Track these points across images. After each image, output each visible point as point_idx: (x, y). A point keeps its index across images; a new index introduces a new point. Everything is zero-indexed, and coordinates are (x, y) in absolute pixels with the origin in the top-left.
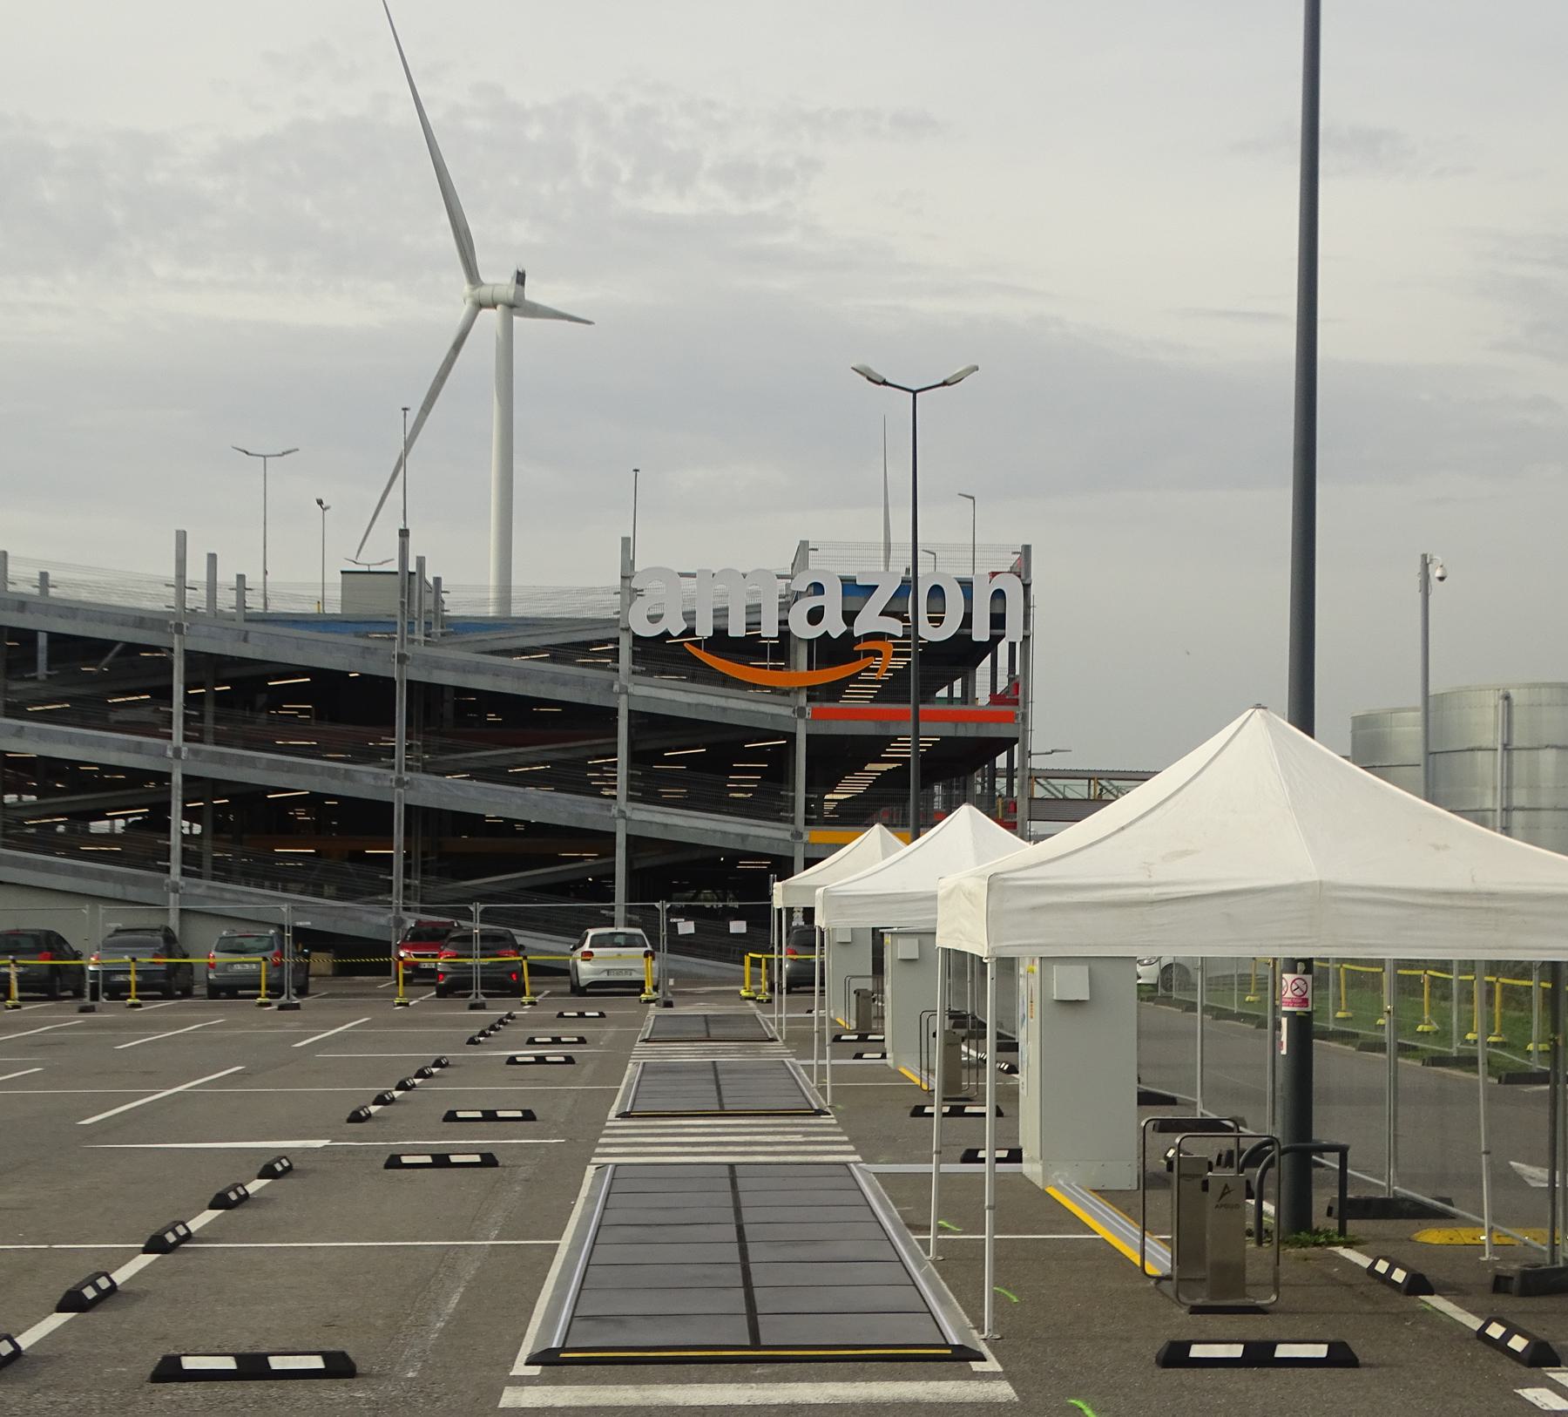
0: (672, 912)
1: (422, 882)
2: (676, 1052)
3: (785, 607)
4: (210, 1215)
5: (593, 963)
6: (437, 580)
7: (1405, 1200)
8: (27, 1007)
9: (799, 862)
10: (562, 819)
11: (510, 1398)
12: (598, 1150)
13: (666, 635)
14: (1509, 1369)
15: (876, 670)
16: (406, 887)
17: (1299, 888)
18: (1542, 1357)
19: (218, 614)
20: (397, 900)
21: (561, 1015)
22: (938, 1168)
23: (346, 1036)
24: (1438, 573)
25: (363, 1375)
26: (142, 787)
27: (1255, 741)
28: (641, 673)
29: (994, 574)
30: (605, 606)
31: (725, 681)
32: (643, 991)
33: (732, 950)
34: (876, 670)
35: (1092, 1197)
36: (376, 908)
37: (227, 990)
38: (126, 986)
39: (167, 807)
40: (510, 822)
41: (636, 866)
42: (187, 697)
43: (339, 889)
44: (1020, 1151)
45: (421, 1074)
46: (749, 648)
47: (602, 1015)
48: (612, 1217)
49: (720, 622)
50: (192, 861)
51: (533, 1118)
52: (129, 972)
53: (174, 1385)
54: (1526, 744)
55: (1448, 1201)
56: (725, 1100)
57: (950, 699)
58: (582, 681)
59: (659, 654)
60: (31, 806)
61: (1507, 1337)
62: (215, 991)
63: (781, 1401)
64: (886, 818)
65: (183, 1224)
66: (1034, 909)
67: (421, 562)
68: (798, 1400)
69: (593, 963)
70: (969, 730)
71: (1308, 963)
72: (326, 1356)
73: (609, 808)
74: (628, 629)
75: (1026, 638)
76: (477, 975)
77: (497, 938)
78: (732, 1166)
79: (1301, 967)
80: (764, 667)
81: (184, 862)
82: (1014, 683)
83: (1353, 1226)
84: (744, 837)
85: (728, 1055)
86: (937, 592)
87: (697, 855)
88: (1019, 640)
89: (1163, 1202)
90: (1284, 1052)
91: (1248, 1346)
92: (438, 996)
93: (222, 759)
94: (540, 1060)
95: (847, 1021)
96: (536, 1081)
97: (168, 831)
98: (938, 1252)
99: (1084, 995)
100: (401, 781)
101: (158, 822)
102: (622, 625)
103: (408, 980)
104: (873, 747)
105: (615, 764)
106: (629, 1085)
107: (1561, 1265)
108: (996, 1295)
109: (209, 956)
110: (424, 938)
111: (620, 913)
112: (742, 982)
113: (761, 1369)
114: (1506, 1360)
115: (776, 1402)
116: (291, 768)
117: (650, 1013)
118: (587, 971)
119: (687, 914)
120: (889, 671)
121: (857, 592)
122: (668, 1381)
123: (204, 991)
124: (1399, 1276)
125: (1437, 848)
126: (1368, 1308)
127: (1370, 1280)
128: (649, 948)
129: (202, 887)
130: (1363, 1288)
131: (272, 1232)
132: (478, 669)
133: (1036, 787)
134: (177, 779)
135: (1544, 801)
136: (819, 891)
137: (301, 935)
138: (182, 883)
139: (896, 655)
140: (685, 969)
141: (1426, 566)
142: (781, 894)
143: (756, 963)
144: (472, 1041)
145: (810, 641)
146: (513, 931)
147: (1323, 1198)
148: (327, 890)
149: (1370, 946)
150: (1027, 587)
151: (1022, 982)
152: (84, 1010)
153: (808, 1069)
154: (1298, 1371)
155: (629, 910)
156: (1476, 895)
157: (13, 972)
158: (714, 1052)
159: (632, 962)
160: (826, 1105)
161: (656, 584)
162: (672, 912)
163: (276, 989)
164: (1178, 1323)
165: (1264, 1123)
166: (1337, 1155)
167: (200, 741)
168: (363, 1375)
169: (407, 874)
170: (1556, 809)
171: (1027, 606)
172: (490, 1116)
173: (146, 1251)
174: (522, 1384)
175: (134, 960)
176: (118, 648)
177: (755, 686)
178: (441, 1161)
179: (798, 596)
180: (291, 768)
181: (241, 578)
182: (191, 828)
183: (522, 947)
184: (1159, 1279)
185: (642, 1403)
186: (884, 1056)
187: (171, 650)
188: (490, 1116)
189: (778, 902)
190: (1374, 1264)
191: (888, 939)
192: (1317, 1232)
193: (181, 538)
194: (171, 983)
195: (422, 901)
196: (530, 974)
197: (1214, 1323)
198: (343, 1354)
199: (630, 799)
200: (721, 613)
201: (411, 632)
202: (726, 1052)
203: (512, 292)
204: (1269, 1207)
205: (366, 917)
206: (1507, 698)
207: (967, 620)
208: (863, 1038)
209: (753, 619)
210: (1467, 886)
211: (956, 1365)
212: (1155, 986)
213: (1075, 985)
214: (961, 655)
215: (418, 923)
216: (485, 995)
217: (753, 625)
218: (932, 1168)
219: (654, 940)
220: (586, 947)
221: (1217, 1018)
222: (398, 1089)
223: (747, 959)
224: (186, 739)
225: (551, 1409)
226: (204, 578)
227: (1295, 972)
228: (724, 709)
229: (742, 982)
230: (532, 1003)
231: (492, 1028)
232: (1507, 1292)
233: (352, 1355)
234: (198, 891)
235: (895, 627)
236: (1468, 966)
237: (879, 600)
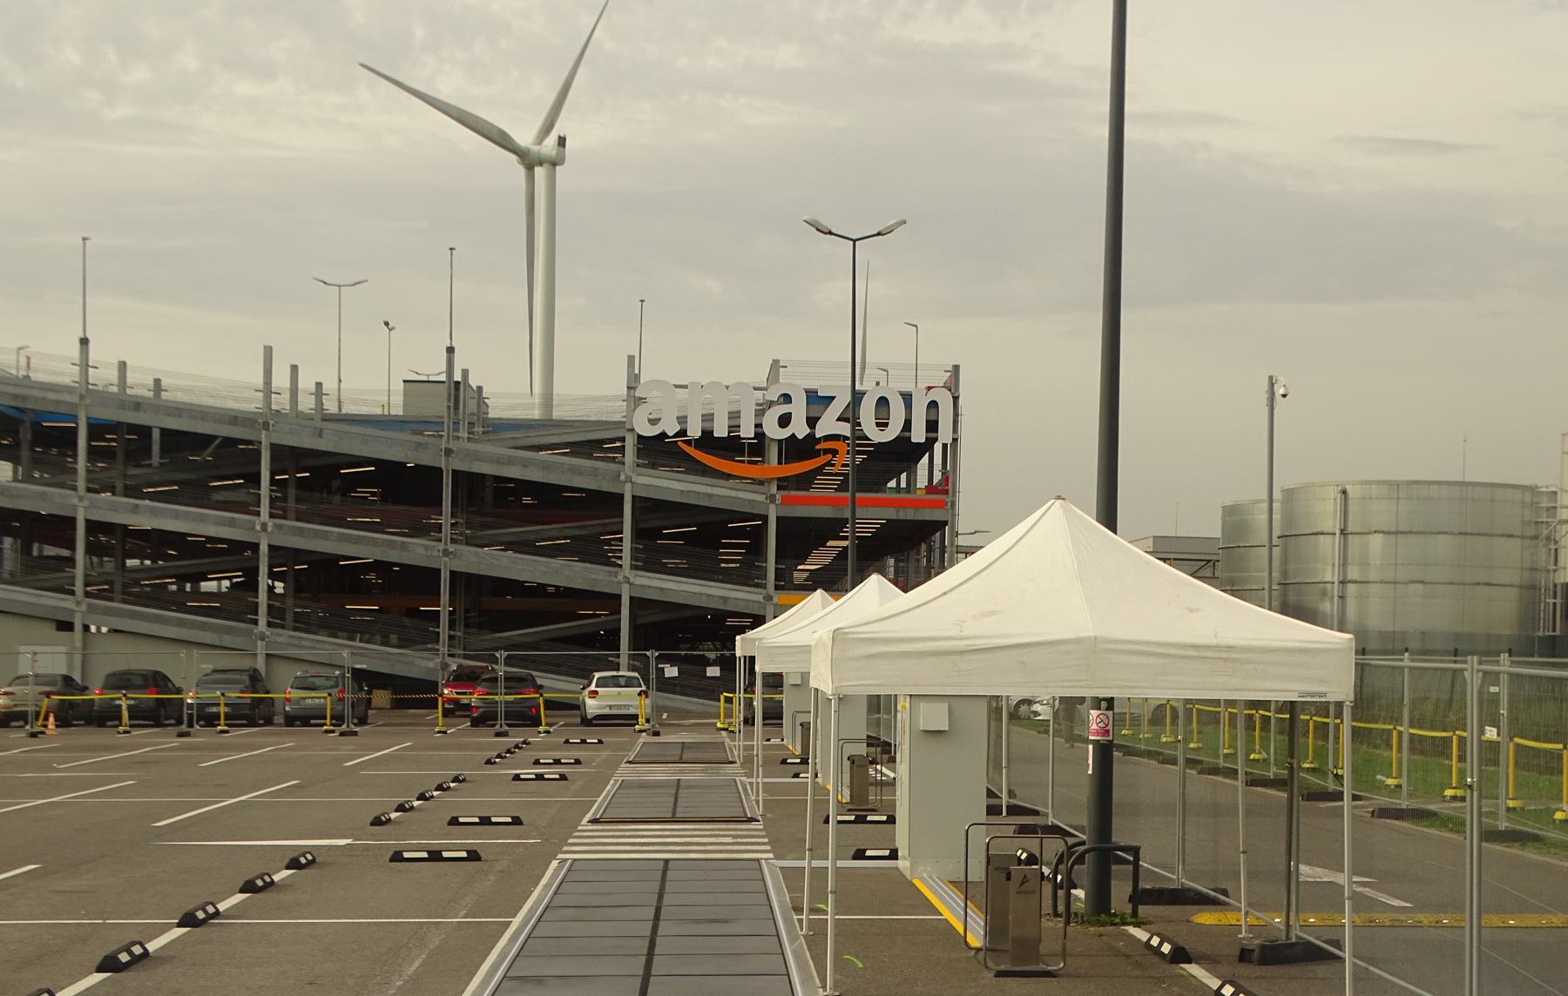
0: (660, 659)
3: (760, 413)
6: (480, 388)
7: (1190, 890)
8: (135, 732)
10: (578, 584)
13: (663, 435)
16: (451, 638)
17: (1078, 641)
19: (300, 415)
20: (443, 648)
21: (567, 742)
22: (834, 864)
23: (390, 755)
24: (1282, 391)
26: (238, 554)
28: (644, 466)
29: (929, 388)
30: (615, 411)
31: (705, 471)
33: (710, 691)
37: (302, 719)
38: (217, 716)
40: (542, 587)
42: (273, 482)
45: (440, 788)
46: (731, 446)
47: (600, 742)
48: (558, 901)
49: (708, 425)
50: (277, 616)
51: (520, 823)
55: (1225, 892)
57: (898, 489)
58: (594, 472)
59: (658, 450)
60: (148, 569)
62: (290, 721)
67: (465, 373)
70: (909, 514)
71: (1110, 702)
75: (955, 440)
76: (501, 709)
77: (521, 680)
78: (667, 861)
79: (1104, 705)
82: (945, 477)
83: (1142, 910)
84: (725, 599)
85: (692, 774)
86: (883, 402)
87: (688, 613)
88: (949, 441)
93: (301, 531)
94: (540, 777)
96: (533, 794)
97: (256, 590)
100: (447, 551)
103: (446, 713)
104: (832, 528)
105: (621, 540)
109: (287, 693)
110: (464, 678)
111: (624, 660)
116: (357, 540)
118: (593, 706)
119: (672, 661)
121: (819, 402)
125: (1191, 610)
126: (1138, 973)
129: (283, 636)
131: (282, 911)
132: (511, 461)
134: (264, 549)
135: (1373, 575)
137: (357, 673)
140: (676, 705)
142: (743, 645)
143: (729, 700)
144: (489, 762)
145: (780, 441)
148: (394, 638)
150: (956, 399)
152: (180, 735)
156: (1218, 648)
157: (124, 704)
158: (682, 772)
160: (759, 812)
161: (655, 393)
162: (660, 659)
163: (338, 719)
169: (452, 625)
171: (956, 415)
172: (485, 821)
173: (179, 925)
177: (729, 477)
178: (435, 856)
179: (771, 404)
180: (357, 540)
181: (319, 385)
183: (541, 687)
184: (978, 950)
188: (485, 821)
189: (738, 653)
193: (268, 351)
194: (255, 714)
199: (634, 567)
200: (708, 418)
203: (554, 153)
204: (1080, 893)
206: (1344, 492)
207: (908, 425)
209: (735, 423)
210: (1211, 641)
213: (936, 717)
214: (904, 453)
215: (460, 666)
217: (734, 427)
218: (805, 864)
220: (593, 687)
224: (272, 516)
226: (288, 385)
227: (1099, 708)
228: (710, 496)
232: (1250, 962)
234: (280, 640)
235: (845, 429)
236: (1231, 703)
237: (836, 408)
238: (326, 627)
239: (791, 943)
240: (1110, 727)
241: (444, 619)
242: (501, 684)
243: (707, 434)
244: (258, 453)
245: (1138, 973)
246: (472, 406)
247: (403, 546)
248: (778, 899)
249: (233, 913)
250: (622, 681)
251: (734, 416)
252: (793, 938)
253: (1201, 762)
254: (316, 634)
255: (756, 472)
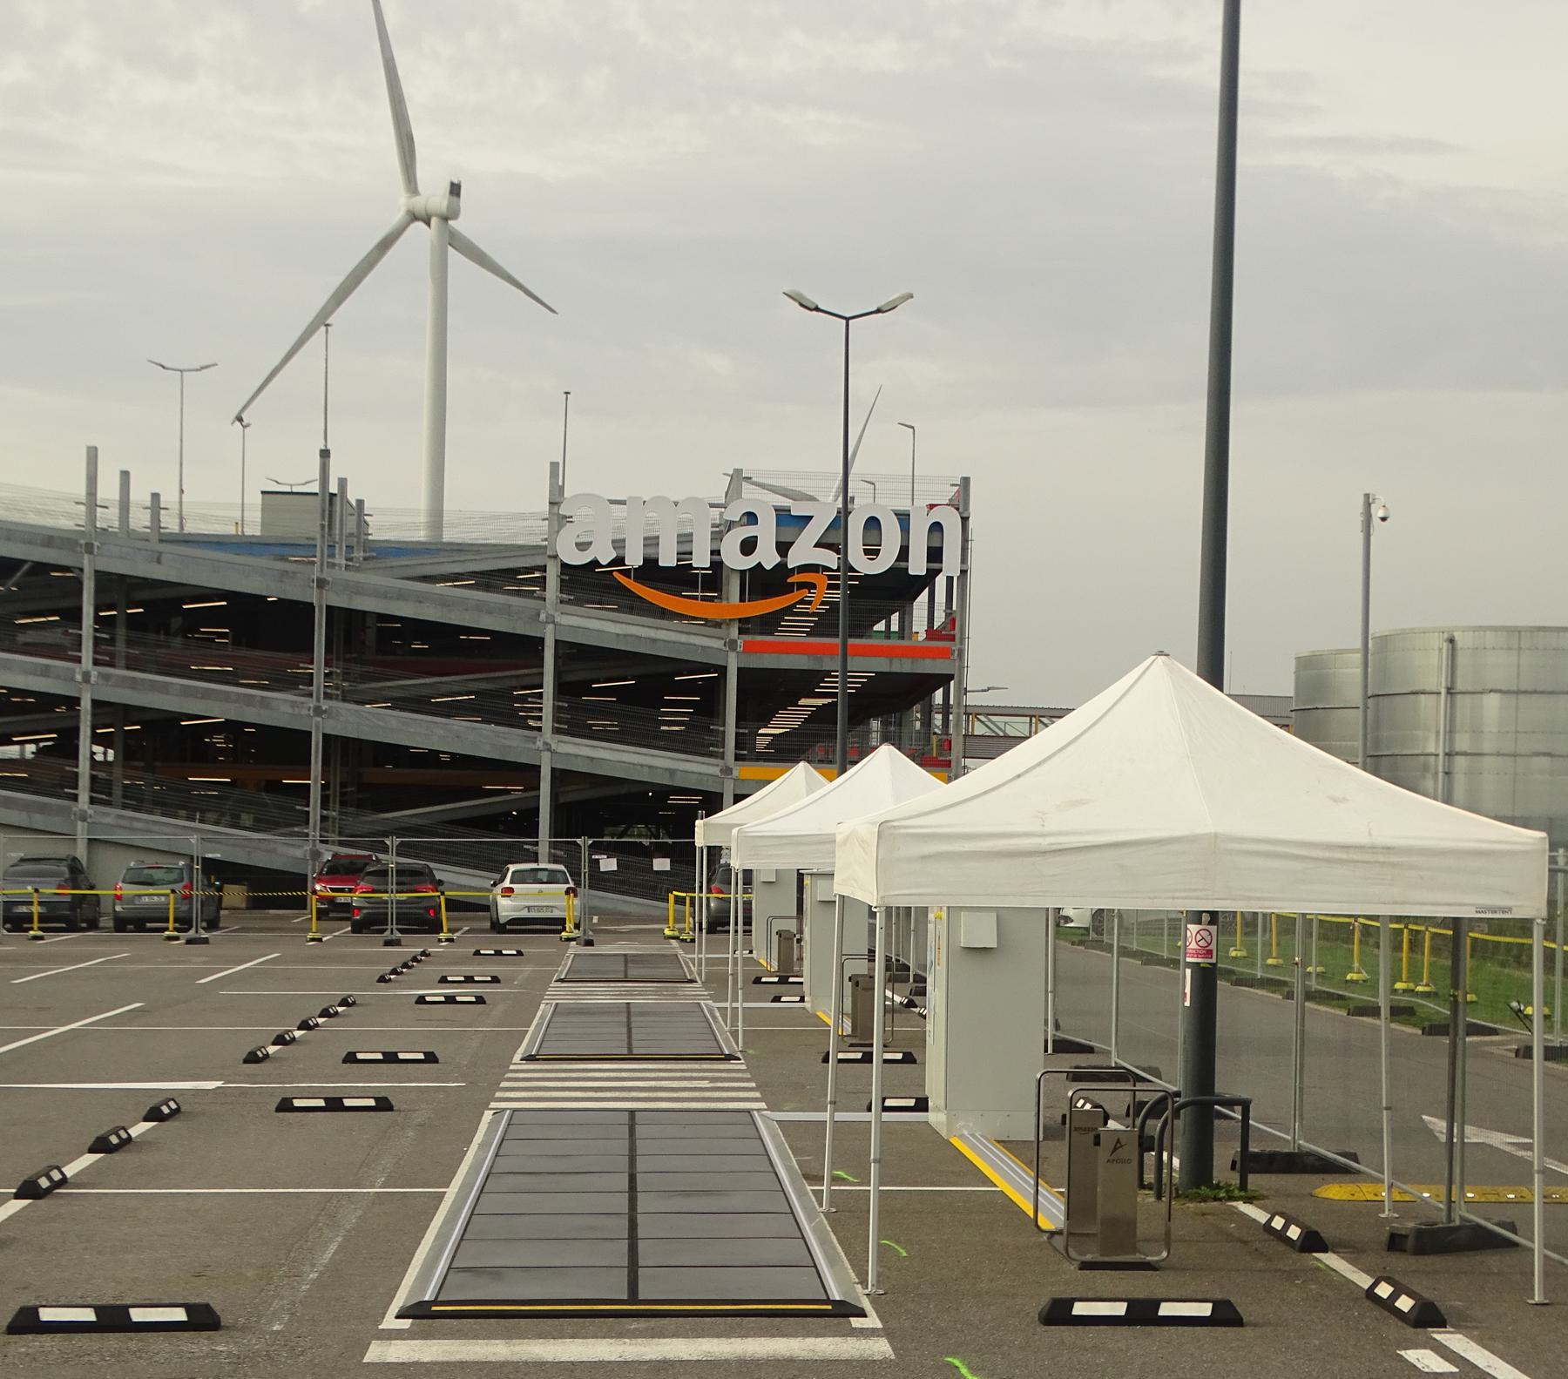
1: (341, 813)
2: (590, 993)
3: (717, 536)
4: (90, 1159)
5: (515, 899)
6: (360, 503)
7: (1309, 1154)
9: (728, 798)
10: (485, 751)
11: (377, 1352)
12: (498, 1094)
13: (595, 563)
14: (1394, 1328)
15: (810, 603)
16: (324, 819)
18: (1428, 1317)
20: (314, 831)
21: (477, 953)
22: (832, 1116)
23: (256, 972)
24: (1381, 514)
25: (227, 1328)
27: (1162, 685)
28: (569, 602)
29: (931, 506)
30: (532, 533)
31: (664, 614)
32: (564, 929)
33: (655, 888)
34: (810, 603)
35: (999, 1151)
36: (295, 840)
37: (135, 922)
38: (28, 918)
39: (75, 731)
41: (562, 800)
42: (98, 619)
43: (256, 820)
44: (926, 1099)
45: (325, 1013)
46: (680, 578)
47: (520, 953)
48: (503, 1165)
49: (651, 551)
50: (101, 789)
51: (436, 1061)
52: (31, 903)
53: (30, 1337)
54: (1470, 689)
56: (635, 1043)
57: (888, 633)
58: (507, 610)
59: (588, 582)
61: (1394, 1296)
62: (121, 924)
63: (654, 1357)
64: (821, 755)
65: (59, 1169)
66: (925, 858)
67: (343, 483)
68: (671, 1356)
69: (515, 899)
70: (904, 666)
71: (1214, 916)
72: (189, 1308)
73: (534, 740)
74: (555, 557)
75: (964, 572)
76: (392, 911)
77: (415, 873)
78: (632, 1112)
79: (1205, 918)
80: (695, 598)
81: (92, 790)
82: (951, 620)
83: (1254, 1180)
84: (672, 772)
85: (643, 997)
86: (873, 524)
87: (624, 790)
88: (956, 574)
89: (1058, 1153)
90: (1187, 1004)
91: (1132, 1304)
92: (353, 931)
93: (133, 684)
94: (450, 1000)
95: (767, 960)
97: (76, 758)
98: (831, 1203)
99: (992, 943)
100: (319, 710)
101: (66, 747)
102: (549, 553)
103: (321, 914)
104: (807, 682)
105: (540, 695)
106: (539, 1026)
107: (1457, 1223)
108: (882, 1251)
109: (115, 886)
110: (341, 871)
111: (543, 849)
112: (666, 921)
113: (634, 1324)
114: (1393, 1320)
115: (647, 1358)
117: (570, 951)
118: (507, 908)
119: (610, 850)
120: (823, 603)
122: (542, 1335)
123: (111, 924)
124: (1294, 1233)
125: (1335, 800)
126: (1260, 1265)
127: (1266, 1236)
128: (572, 885)
129: (110, 815)
130: (1258, 1245)
131: (150, 1178)
132: (401, 596)
133: (977, 724)
134: (86, 705)
135: (1488, 746)
136: (735, 831)
137: (210, 866)
138: (90, 812)
139: (830, 587)
141: (1368, 505)
142: (704, 832)
143: (680, 901)
144: (382, 979)
145: (742, 572)
146: (432, 865)
147: (1224, 1153)
148: (247, 819)
149: (1264, 899)
150: (965, 520)
151: (931, 927)
153: (723, 1010)
154: (1181, 1329)
155: (553, 845)
156: (1373, 848)
158: (629, 993)
159: (552, 898)
160: (737, 1049)
161: (585, 511)
162: (596, 848)
164: (1065, 1278)
165: (1174, 1079)
166: (1239, 1108)
167: (112, 665)
168: (227, 1328)
169: (325, 803)
170: (1499, 755)
171: (965, 540)
172: (391, 1058)
173: (17, 1196)
174: (389, 1339)
175: (37, 890)
176: (26, 567)
177: (681, 617)
178: (334, 1104)
179: (731, 525)
180: (206, 695)
181: (155, 496)
182: (105, 754)
183: (441, 882)
184: (1052, 1234)
185: (510, 1359)
186: (802, 1000)
187: (81, 570)
188: (391, 1058)
189: (699, 841)
190: (1271, 1219)
191: (807, 881)
192: (1218, 1187)
193: (92, 455)
194: (75, 916)
195: (340, 834)
196: (447, 910)
197: (1103, 1279)
198: (207, 1306)
199: (556, 731)
200: (652, 542)
201: (332, 555)
202: (642, 993)
203: (445, 204)
205: (281, 849)
206: (1452, 641)
207: (904, 553)
208: (783, 980)
209: (685, 548)
210: (1361, 838)
211: (836, 1321)
212: (1087, 929)
214: (898, 588)
215: (335, 856)
216: (401, 931)
217: (685, 554)
218: (826, 1116)
219: (576, 875)
220: (507, 884)
221: (1145, 963)
222: (299, 1028)
223: (671, 897)
224: (96, 663)
225: (417, 1364)
226: (117, 497)
228: (654, 641)
229: (666, 921)
230: (450, 940)
231: (405, 965)
232: (1403, 1250)
233: (217, 1308)
235: (830, 559)
237: (814, 531)
238: (163, 804)
239: (810, 1221)
240: (1213, 947)
241: (315, 795)
242: (393, 879)
243: (650, 563)
244: (79, 583)
245: (1260, 1265)
246: (351, 525)
247: (264, 703)
248: (784, 1166)
249: (84, 1179)
250: (543, 876)
251: (685, 539)
252: (811, 1216)
253: (1233, 972)
254: (151, 813)
255: (711, 611)
